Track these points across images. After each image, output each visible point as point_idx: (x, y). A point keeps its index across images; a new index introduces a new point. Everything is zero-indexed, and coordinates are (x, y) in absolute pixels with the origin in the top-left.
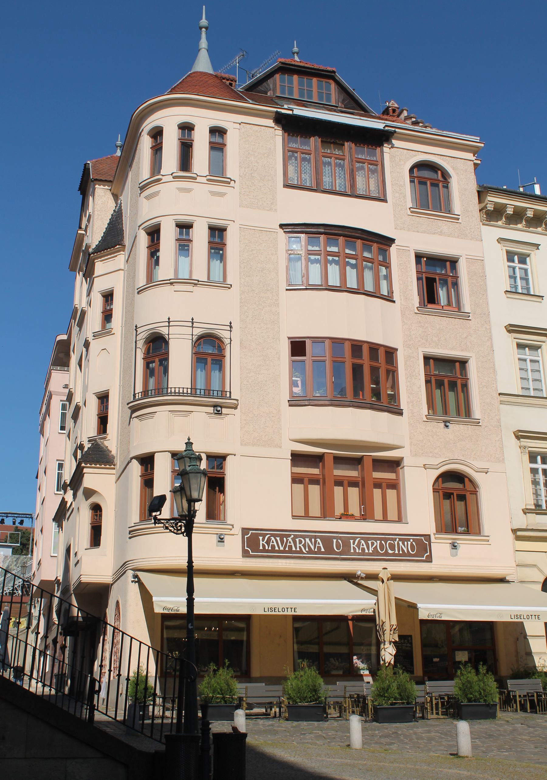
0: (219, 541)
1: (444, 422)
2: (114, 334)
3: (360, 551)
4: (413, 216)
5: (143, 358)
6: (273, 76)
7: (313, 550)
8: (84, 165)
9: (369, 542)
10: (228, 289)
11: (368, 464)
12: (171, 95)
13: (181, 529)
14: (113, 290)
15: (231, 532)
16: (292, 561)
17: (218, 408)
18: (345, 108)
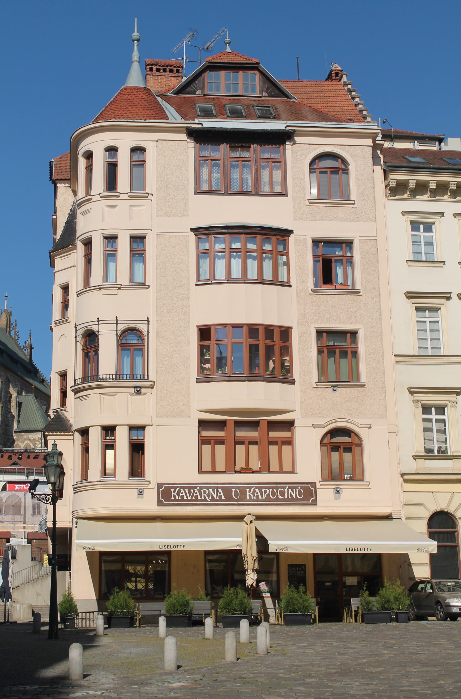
0: (139, 494)
1: (332, 387)
2: (70, 322)
3: (255, 498)
4: (311, 206)
5: (82, 350)
6: (201, 75)
7: (215, 498)
8: (49, 163)
9: (262, 490)
10: (146, 289)
11: (264, 426)
12: (97, 124)
13: (49, 501)
14: (69, 284)
15: (149, 487)
16: (198, 508)
17: (138, 390)
18: (269, 96)
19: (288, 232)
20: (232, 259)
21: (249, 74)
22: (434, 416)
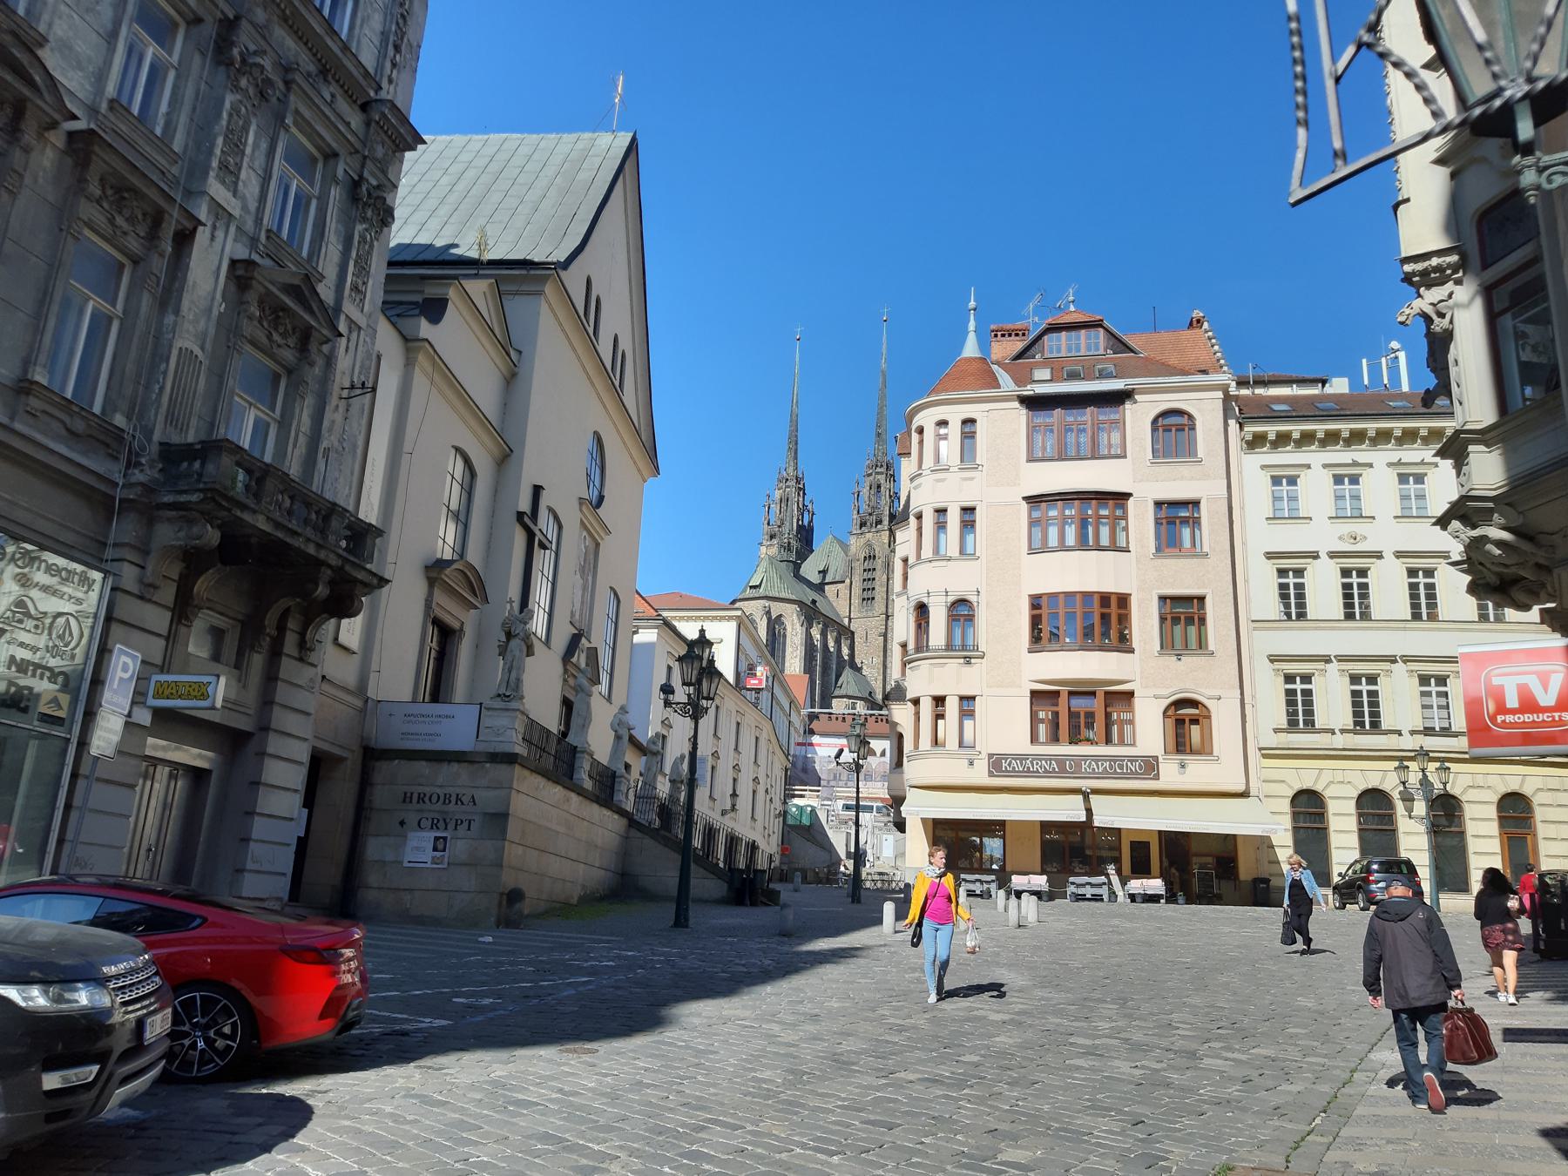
17: (968, 660)
19: (1127, 496)
20: (1101, 527)
21: (1092, 332)
22: (1433, 688)
